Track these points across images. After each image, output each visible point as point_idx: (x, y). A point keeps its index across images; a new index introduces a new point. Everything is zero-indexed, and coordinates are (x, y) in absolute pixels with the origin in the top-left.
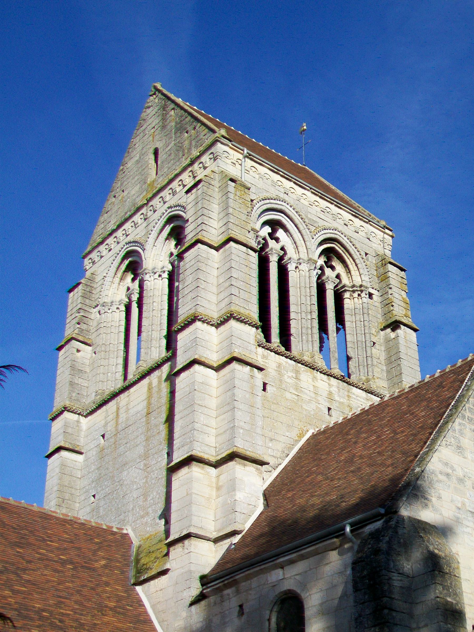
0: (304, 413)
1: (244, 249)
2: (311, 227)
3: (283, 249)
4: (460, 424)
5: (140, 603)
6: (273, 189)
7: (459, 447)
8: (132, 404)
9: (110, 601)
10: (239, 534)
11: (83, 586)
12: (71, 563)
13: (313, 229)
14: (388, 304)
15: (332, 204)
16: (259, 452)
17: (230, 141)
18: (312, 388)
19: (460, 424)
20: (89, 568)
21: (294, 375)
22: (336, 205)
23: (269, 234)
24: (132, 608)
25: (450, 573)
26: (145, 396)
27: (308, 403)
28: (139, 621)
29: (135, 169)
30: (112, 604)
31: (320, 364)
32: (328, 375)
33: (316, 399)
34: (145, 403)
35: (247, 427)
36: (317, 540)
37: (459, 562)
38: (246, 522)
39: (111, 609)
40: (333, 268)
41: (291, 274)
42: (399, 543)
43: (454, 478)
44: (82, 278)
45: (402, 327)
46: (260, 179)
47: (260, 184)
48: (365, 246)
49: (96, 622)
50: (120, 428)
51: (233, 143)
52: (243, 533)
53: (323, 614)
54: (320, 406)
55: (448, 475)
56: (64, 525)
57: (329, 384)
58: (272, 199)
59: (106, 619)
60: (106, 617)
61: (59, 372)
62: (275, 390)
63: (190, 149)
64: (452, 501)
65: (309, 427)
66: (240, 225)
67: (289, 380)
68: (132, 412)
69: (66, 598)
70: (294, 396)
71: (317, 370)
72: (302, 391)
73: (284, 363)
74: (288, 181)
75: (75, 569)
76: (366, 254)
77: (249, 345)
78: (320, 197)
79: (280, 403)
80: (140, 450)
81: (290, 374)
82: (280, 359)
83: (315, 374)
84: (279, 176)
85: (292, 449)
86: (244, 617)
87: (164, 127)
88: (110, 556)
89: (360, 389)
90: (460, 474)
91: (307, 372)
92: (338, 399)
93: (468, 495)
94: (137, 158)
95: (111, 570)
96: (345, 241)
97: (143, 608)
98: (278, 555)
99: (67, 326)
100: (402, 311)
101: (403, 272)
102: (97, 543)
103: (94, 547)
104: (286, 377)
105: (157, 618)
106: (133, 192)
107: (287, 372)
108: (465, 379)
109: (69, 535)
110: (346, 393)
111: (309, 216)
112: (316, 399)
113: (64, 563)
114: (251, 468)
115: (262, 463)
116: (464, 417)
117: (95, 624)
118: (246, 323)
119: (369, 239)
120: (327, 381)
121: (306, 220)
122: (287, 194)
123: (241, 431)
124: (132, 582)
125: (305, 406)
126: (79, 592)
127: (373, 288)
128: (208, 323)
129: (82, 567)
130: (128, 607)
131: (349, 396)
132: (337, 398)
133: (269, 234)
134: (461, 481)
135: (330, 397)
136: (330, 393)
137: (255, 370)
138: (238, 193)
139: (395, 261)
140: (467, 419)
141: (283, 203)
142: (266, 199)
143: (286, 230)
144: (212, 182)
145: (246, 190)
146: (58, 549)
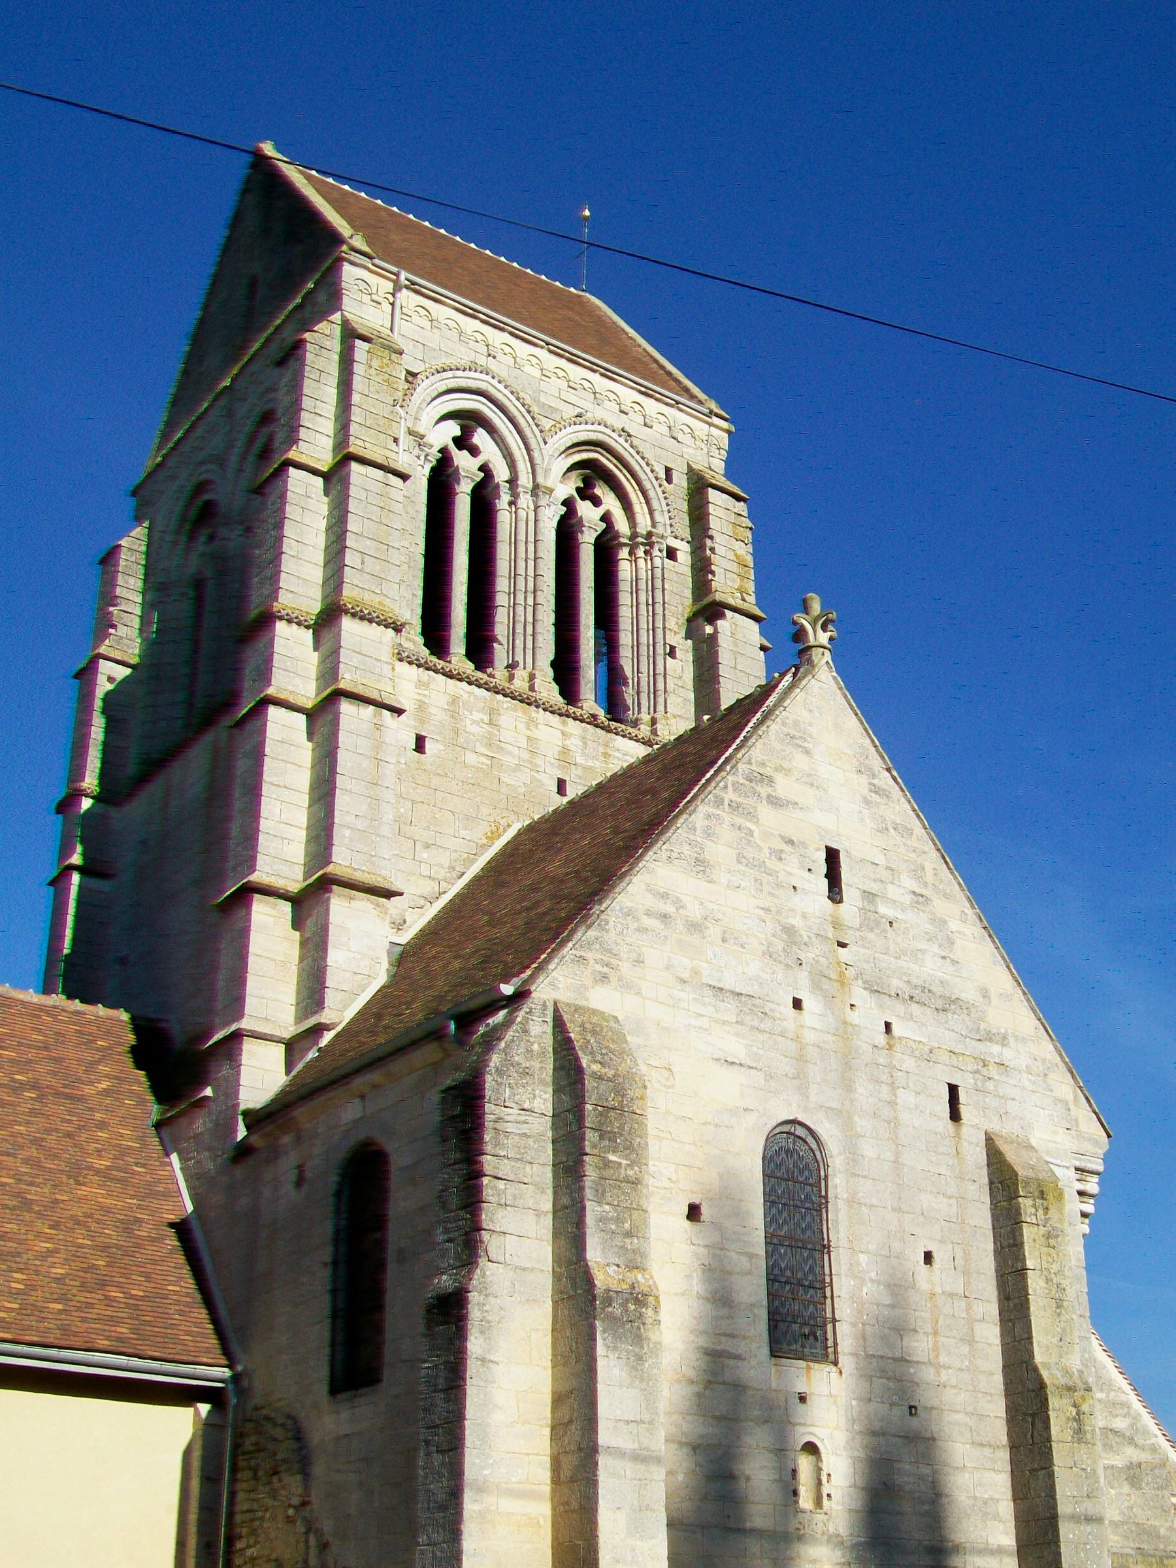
1: (379, 474)
3: (484, 468)
4: (708, 816)
6: (463, 349)
7: (699, 861)
9: (100, 1157)
10: (329, 1030)
11: (48, 1131)
12: (34, 1086)
13: (547, 424)
14: (702, 568)
16: (383, 872)
17: (370, 258)
18: (523, 743)
19: (708, 816)
21: (486, 718)
22: (602, 375)
24: (143, 1170)
25: (622, 1106)
27: (514, 770)
28: (153, 1194)
31: (545, 694)
32: (561, 715)
33: (531, 763)
35: (360, 824)
37: (645, 1087)
38: (346, 1007)
39: (98, 1172)
40: (596, 502)
42: (529, 1051)
43: (678, 921)
44: (121, 538)
45: (728, 613)
46: (435, 330)
47: (433, 339)
48: (665, 453)
49: (58, 1197)
51: (376, 261)
52: (339, 1028)
55: (665, 917)
57: (563, 733)
58: (458, 369)
59: (83, 1191)
60: (84, 1188)
62: (442, 748)
64: (668, 967)
65: (513, 817)
66: (376, 427)
67: (474, 729)
69: (8, 1154)
70: (483, 759)
71: (537, 707)
72: (502, 749)
73: (465, 696)
74: (496, 331)
75: (40, 1098)
77: (378, 664)
78: (569, 360)
79: (450, 775)
81: (477, 716)
82: (456, 686)
83: (534, 715)
84: (478, 322)
85: (473, 861)
86: (305, 1188)
88: (121, 1072)
89: (631, 739)
90: (694, 912)
91: (515, 710)
92: (583, 762)
95: (117, 1099)
96: (619, 444)
97: (169, 1168)
100: (733, 581)
101: (742, 503)
102: (103, 1049)
103: (90, 1056)
104: (468, 722)
107: (471, 712)
108: (749, 721)
109: (45, 1035)
110: (601, 749)
111: (543, 399)
112: (531, 763)
114: (364, 903)
115: (388, 894)
116: (719, 802)
117: (56, 1201)
118: (371, 621)
119: (677, 435)
120: (561, 727)
122: (494, 357)
123: (347, 833)
125: (505, 778)
126: (36, 1142)
127: (676, 537)
128: (299, 624)
129: (58, 1094)
130: (136, 1168)
131: (606, 755)
132: (580, 760)
134: (695, 927)
136: (565, 750)
137: (386, 713)
138: (376, 363)
140: (726, 806)
141: (483, 376)
142: (444, 371)
143: (491, 430)
144: (328, 343)
145: (394, 356)
146: (12, 1061)
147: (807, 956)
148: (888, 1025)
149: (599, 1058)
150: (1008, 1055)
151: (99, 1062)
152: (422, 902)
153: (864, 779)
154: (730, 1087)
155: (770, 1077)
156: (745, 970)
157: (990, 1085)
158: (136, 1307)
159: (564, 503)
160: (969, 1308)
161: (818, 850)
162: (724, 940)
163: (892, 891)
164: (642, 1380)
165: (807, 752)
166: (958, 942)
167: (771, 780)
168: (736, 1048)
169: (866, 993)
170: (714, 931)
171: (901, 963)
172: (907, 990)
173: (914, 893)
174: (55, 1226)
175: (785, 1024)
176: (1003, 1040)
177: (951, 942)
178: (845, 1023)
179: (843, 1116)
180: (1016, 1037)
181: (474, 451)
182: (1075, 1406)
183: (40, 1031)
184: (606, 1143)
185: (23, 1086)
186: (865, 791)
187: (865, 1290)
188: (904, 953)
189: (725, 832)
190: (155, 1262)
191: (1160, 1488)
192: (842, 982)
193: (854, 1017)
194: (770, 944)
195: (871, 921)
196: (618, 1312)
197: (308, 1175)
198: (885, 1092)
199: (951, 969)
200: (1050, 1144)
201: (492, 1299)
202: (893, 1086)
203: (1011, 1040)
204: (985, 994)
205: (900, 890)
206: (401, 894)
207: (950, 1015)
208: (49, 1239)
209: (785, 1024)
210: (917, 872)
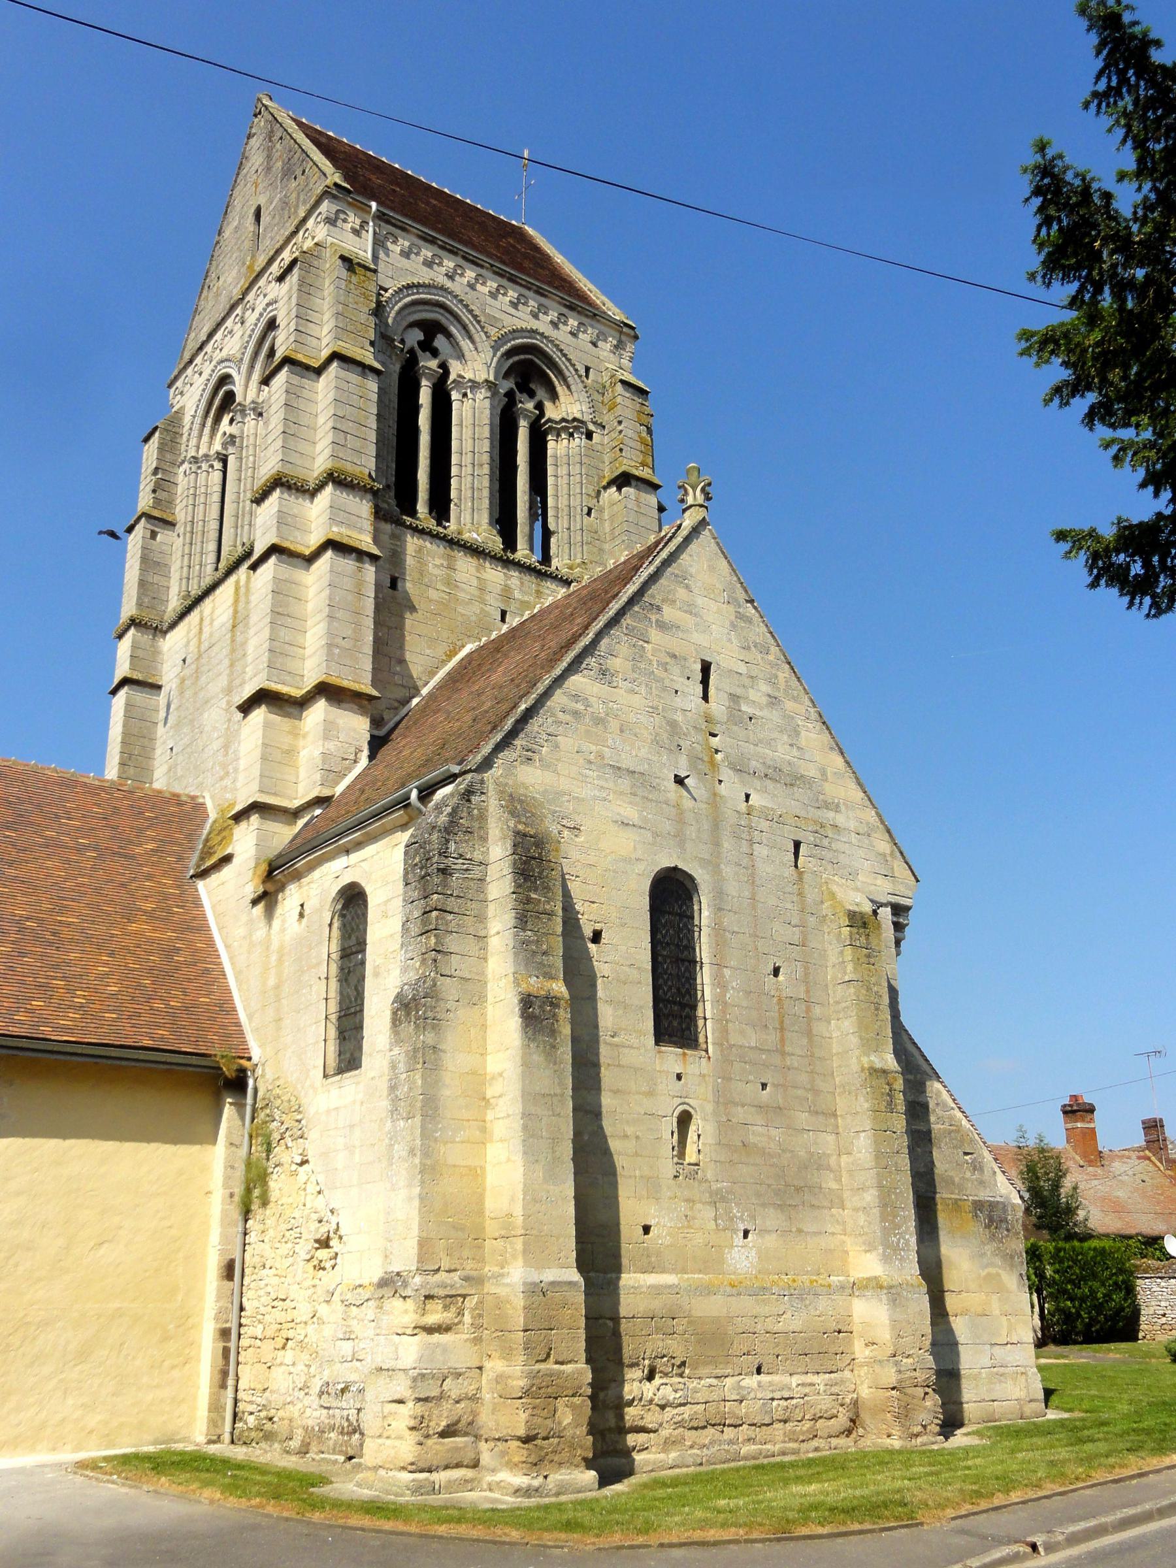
0: (460, 618)
2: (489, 328)
5: (197, 902)
7: (603, 673)
8: (217, 612)
15: (529, 289)
18: (475, 582)
23: (419, 343)
26: (231, 601)
27: (467, 604)
29: (233, 241)
30: (149, 906)
34: (231, 611)
38: (337, 783)
39: (145, 912)
50: (203, 648)
54: (488, 608)
55: (576, 714)
56: (99, 794)
59: (134, 927)
61: (127, 566)
63: (297, 206)
65: (466, 640)
67: (436, 572)
68: (216, 624)
70: (443, 595)
72: (457, 586)
76: (587, 369)
80: (223, 681)
81: (438, 562)
86: (304, 920)
87: (268, 169)
90: (599, 708)
93: (610, 741)
94: (235, 223)
99: (141, 494)
105: (217, 923)
106: (230, 280)
113: (81, 849)
121: (482, 319)
124: (192, 872)
133: (419, 343)
134: (599, 721)
135: (506, 594)
139: (638, 378)
145: (369, 274)
146: (78, 829)
147: (685, 744)
148: (747, 796)
149: (524, 820)
150: (840, 819)
151: (148, 828)
152: (396, 704)
153: (731, 608)
154: (624, 843)
155: (656, 835)
156: (635, 753)
157: (825, 842)
158: (173, 1015)
159: (506, 395)
160: (808, 1010)
161: (695, 662)
162: (622, 731)
163: (752, 694)
164: (555, 1064)
165: (687, 587)
166: (803, 733)
167: (659, 609)
168: (630, 813)
169: (731, 772)
170: (614, 725)
171: (759, 749)
172: (762, 770)
173: (769, 696)
174: (111, 954)
175: (669, 795)
176: (837, 809)
177: (798, 734)
178: (715, 794)
179: (714, 865)
180: (847, 807)
181: (435, 353)
182: (888, 1084)
183: (99, 805)
184: (529, 884)
185: (86, 848)
186: (733, 618)
187: (728, 996)
188: (761, 741)
189: (624, 649)
190: (189, 980)
191: (955, 1147)
192: (713, 764)
193: (723, 789)
194: (657, 734)
195: (740, 719)
196: (537, 1011)
197: (307, 912)
198: (745, 848)
199: (795, 752)
200: (873, 887)
201: (442, 1003)
202: (751, 842)
203: (843, 808)
204: (823, 773)
205: (758, 693)
206: (100, 533)
207: (796, 789)
208: (106, 964)
209: (669, 795)
210: (772, 681)
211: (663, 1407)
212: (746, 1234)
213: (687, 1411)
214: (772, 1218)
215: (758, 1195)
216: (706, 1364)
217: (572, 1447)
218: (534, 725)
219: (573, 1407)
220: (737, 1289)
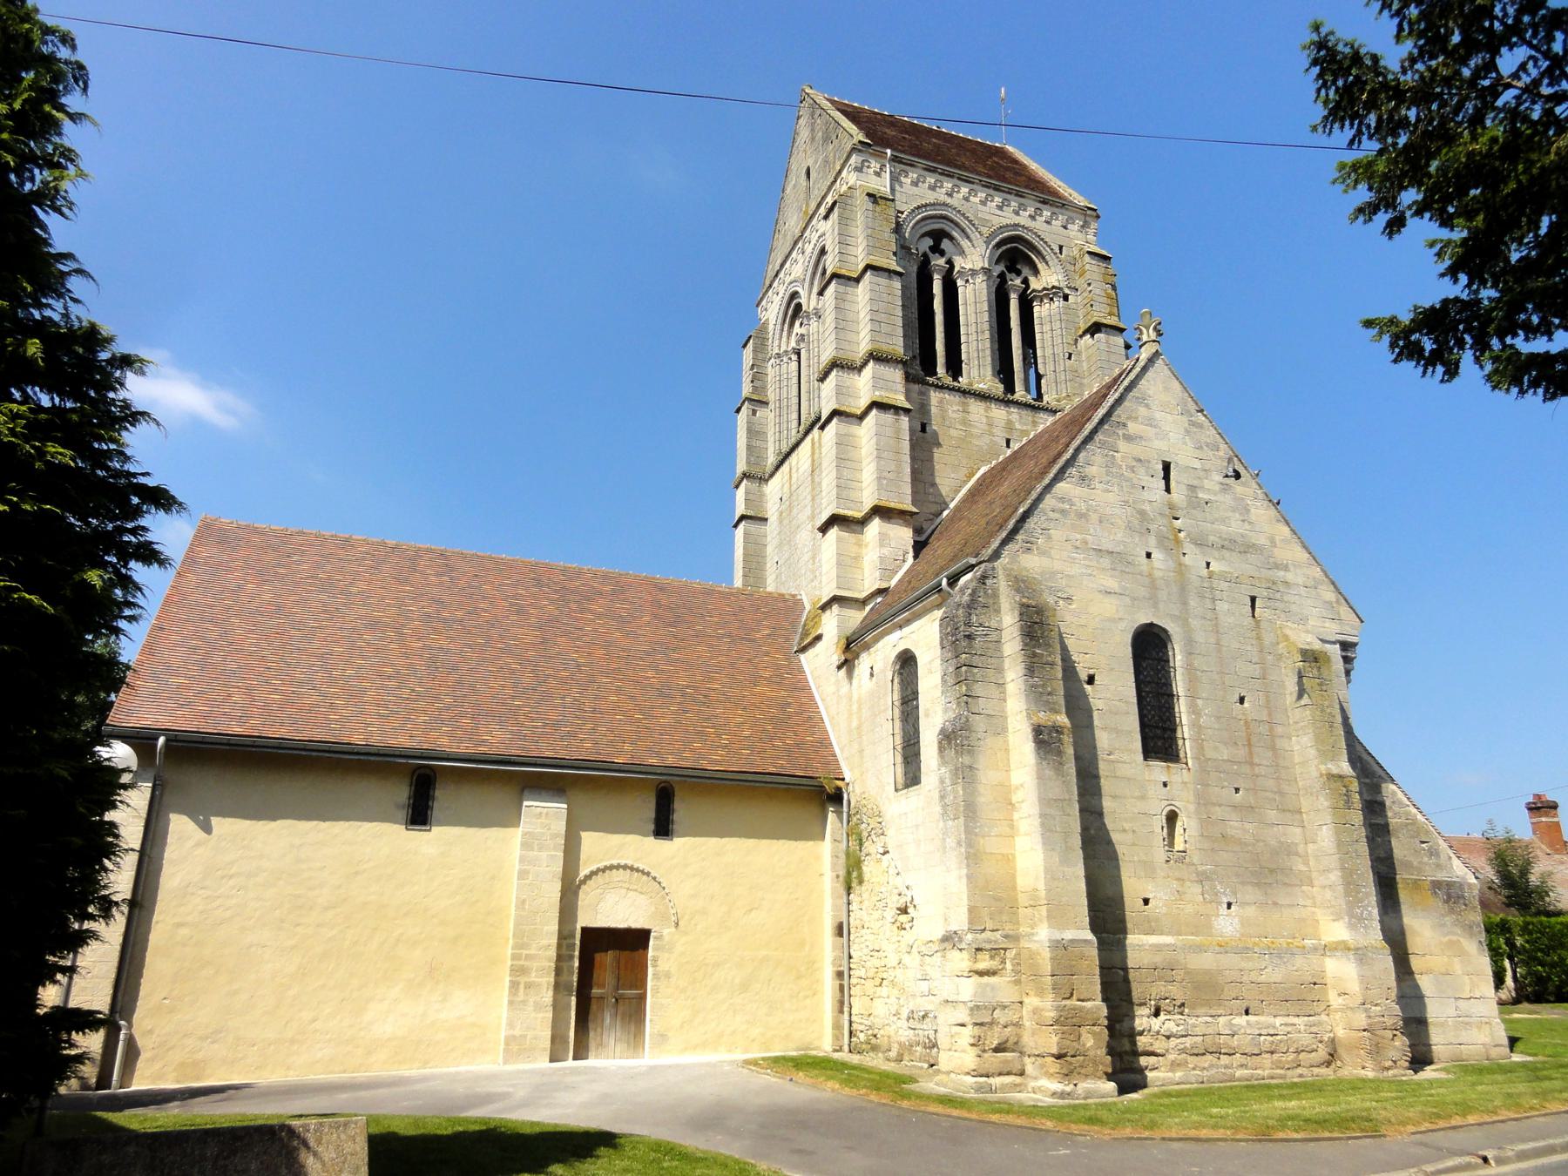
20: (749, 640)
36: (318, 759)
41: (960, 290)
53: (523, 790)
55: (1063, 511)
87: (813, 139)
98: (895, 615)
113: (720, 637)
132: (1018, 426)
135: (1009, 426)
150: (1290, 577)
154: (1109, 607)
168: (1112, 584)
179: (1184, 621)
211: (1168, 1037)
212: (1229, 905)
213: (1188, 1041)
214: (1251, 894)
215: (1237, 875)
216: (1202, 1005)
217: (1094, 1063)
218: (1031, 523)
219: (1094, 1034)
220: (1223, 948)
